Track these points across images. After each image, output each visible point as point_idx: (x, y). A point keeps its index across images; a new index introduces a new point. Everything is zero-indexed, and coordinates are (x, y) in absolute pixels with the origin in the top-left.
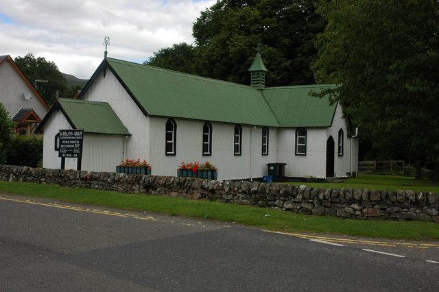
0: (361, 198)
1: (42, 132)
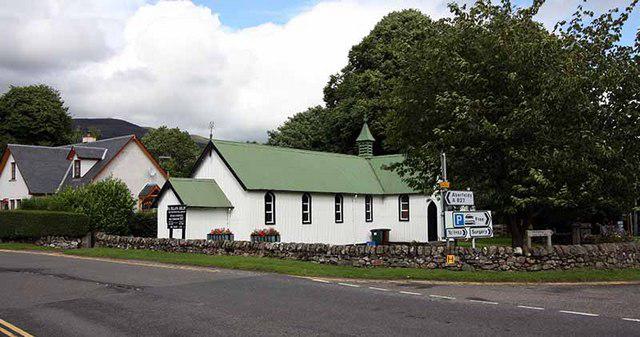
1: (157, 207)
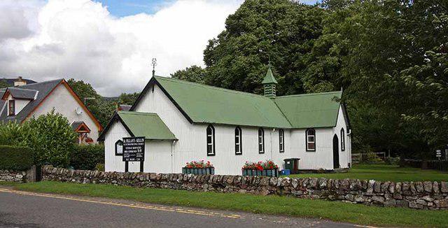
0: (433, 190)
